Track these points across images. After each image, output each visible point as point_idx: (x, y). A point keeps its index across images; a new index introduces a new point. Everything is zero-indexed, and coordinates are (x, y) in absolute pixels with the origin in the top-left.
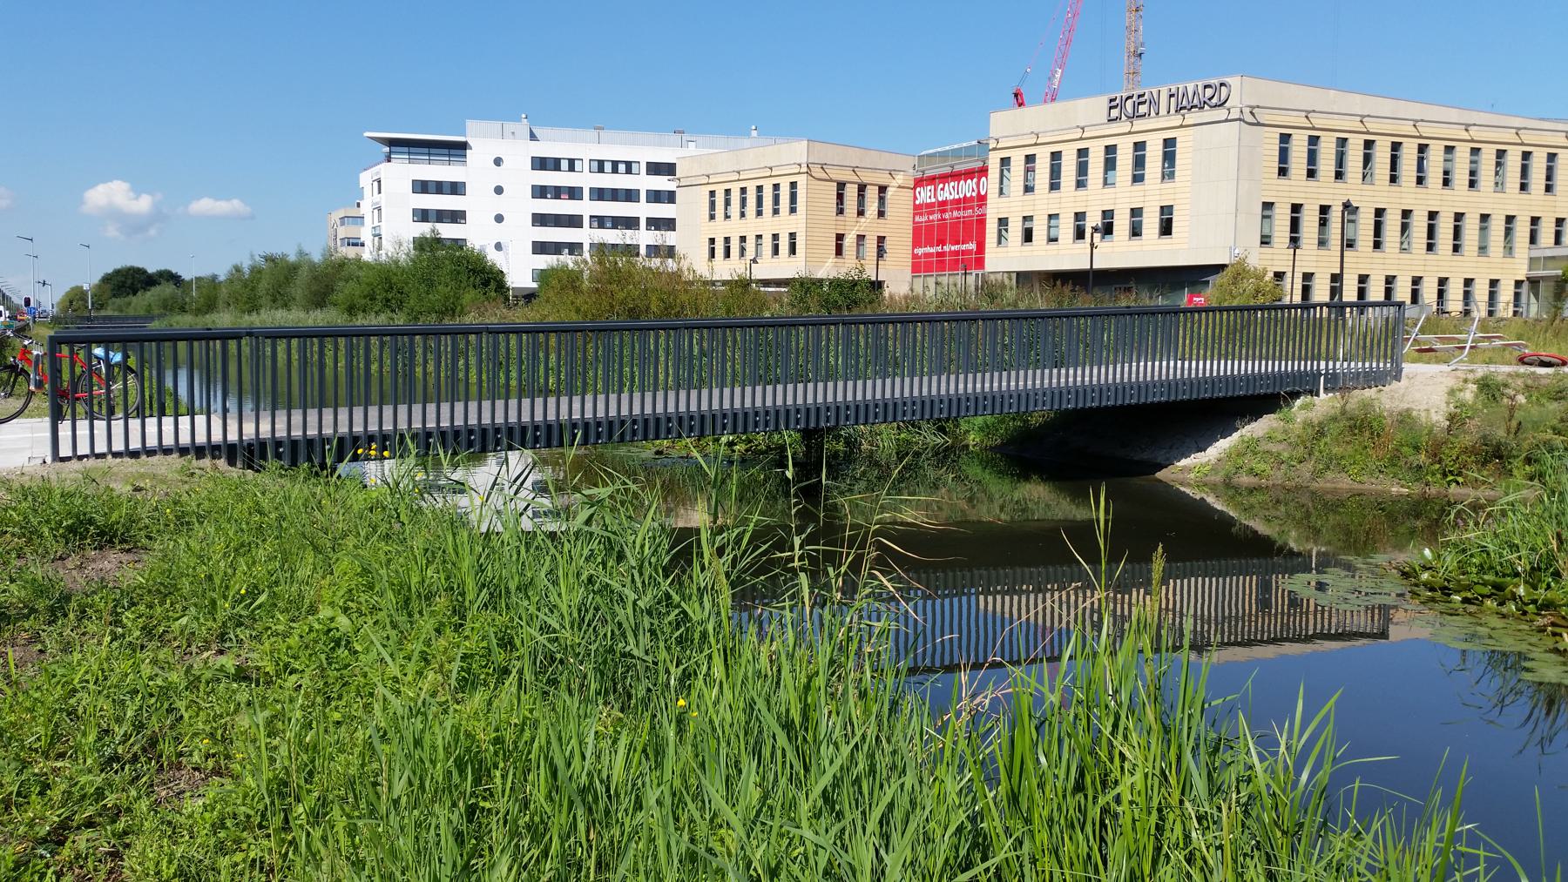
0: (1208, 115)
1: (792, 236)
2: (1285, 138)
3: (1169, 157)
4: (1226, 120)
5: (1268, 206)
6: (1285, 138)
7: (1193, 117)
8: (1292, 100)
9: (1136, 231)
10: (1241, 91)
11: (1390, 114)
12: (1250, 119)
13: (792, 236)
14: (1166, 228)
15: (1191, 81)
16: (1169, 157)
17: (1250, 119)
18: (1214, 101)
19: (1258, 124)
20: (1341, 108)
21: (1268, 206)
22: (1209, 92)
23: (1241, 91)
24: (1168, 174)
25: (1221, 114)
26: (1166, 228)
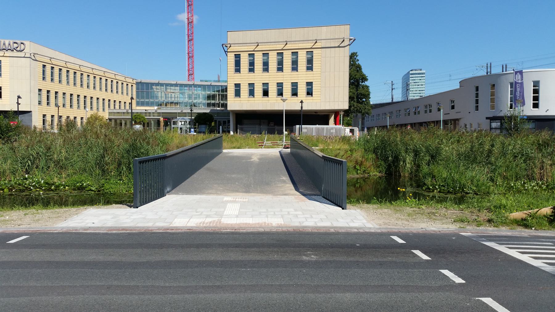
0: (15, 54)
1: (238, 70)
2: (44, 66)
3: (310, 62)
4: (24, 57)
5: (40, 90)
6: (44, 66)
7: (8, 53)
8: (46, 52)
9: (280, 93)
10: (30, 47)
11: (74, 62)
12: (33, 58)
13: (238, 70)
14: (310, 93)
15: (7, 39)
16: (310, 62)
17: (33, 58)
18: (18, 49)
19: (36, 60)
20: (61, 58)
21: (40, 90)
22: (16, 45)
23: (30, 47)
24: (310, 68)
25: (22, 54)
26: (310, 93)
